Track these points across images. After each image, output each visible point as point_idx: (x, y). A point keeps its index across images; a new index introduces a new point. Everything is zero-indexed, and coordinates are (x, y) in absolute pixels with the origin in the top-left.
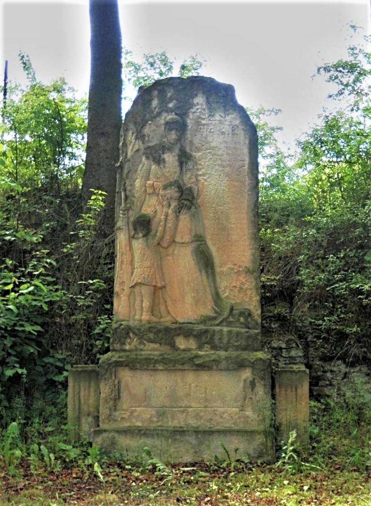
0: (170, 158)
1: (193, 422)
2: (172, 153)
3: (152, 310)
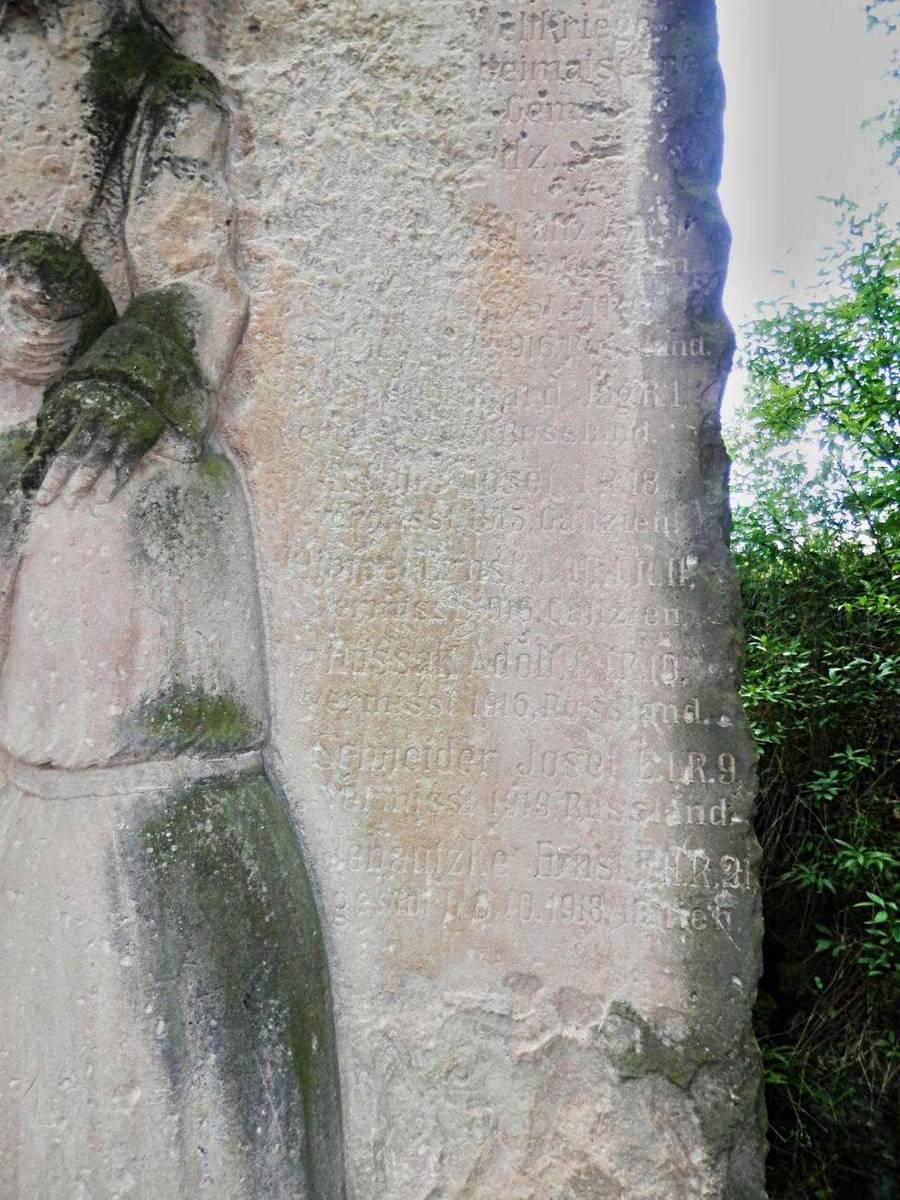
2: (42, 30)
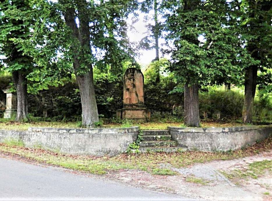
0: (132, 80)
1: (136, 117)
3: (130, 102)
